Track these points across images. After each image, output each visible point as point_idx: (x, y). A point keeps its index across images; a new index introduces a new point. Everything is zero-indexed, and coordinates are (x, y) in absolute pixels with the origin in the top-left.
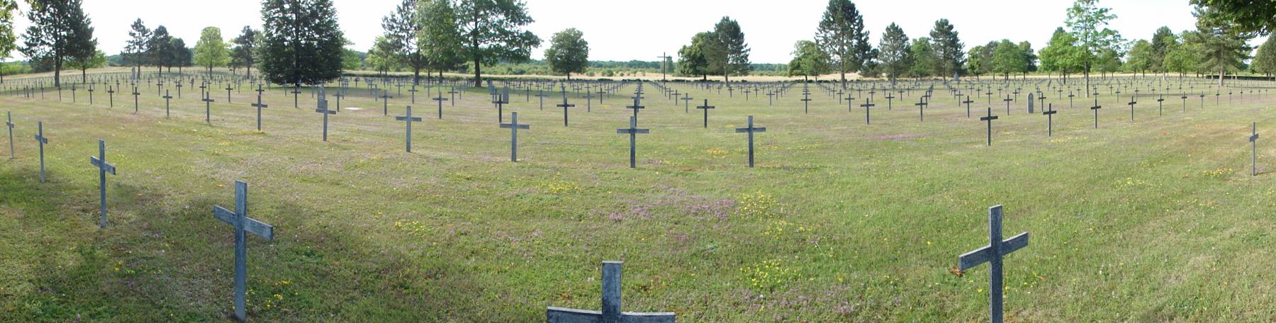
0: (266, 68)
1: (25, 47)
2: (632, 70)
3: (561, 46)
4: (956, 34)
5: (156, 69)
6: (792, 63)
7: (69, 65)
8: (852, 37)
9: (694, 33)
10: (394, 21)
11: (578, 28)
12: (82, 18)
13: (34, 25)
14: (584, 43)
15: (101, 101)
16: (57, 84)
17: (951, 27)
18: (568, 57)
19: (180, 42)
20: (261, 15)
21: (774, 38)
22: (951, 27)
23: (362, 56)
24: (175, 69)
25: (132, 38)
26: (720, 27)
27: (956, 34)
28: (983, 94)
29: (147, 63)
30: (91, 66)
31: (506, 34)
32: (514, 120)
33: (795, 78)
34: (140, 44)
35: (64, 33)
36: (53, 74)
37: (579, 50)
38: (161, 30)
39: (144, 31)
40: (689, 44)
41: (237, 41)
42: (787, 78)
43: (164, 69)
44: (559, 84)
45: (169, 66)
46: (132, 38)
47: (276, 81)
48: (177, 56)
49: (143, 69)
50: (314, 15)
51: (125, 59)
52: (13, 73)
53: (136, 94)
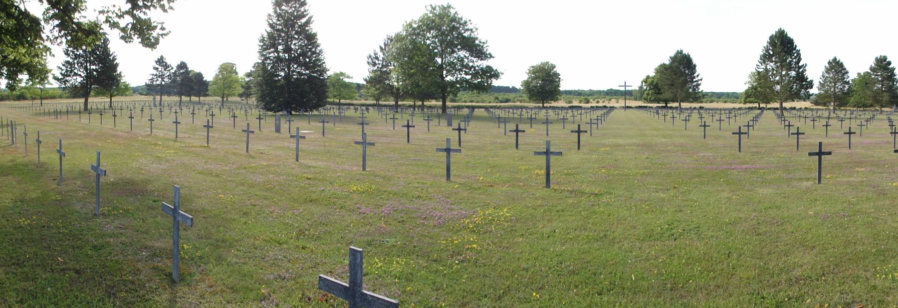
0: (262, 98)
1: (60, 77)
2: (608, 97)
3: (536, 78)
4: (894, 69)
5: (176, 98)
6: (747, 92)
7: (98, 94)
8: (790, 69)
9: (657, 64)
10: (377, 58)
11: (551, 62)
12: (109, 55)
13: (69, 59)
14: (557, 75)
15: (123, 124)
16: (86, 108)
17: (889, 63)
18: (542, 87)
19: (200, 75)
20: (258, 54)
21: (727, 70)
22: (889, 63)
23: (359, 86)
24: (194, 99)
25: (155, 72)
26: (674, 59)
27: (894, 69)
28: (243, 112)
29: (169, 94)
30: (117, 95)
31: (467, 66)
32: (816, 154)
33: (748, 105)
34: (162, 77)
35: (93, 67)
36: (83, 100)
37: (552, 81)
38: (183, 66)
39: (166, 66)
40: (652, 74)
41: (249, 75)
42: (742, 105)
43: (184, 98)
44: (695, 115)
45: (190, 96)
46: (155, 72)
47: (271, 110)
48: (196, 87)
49: (165, 98)
50: (304, 54)
51: (150, 89)
52: (53, 97)
53: (131, 118)
